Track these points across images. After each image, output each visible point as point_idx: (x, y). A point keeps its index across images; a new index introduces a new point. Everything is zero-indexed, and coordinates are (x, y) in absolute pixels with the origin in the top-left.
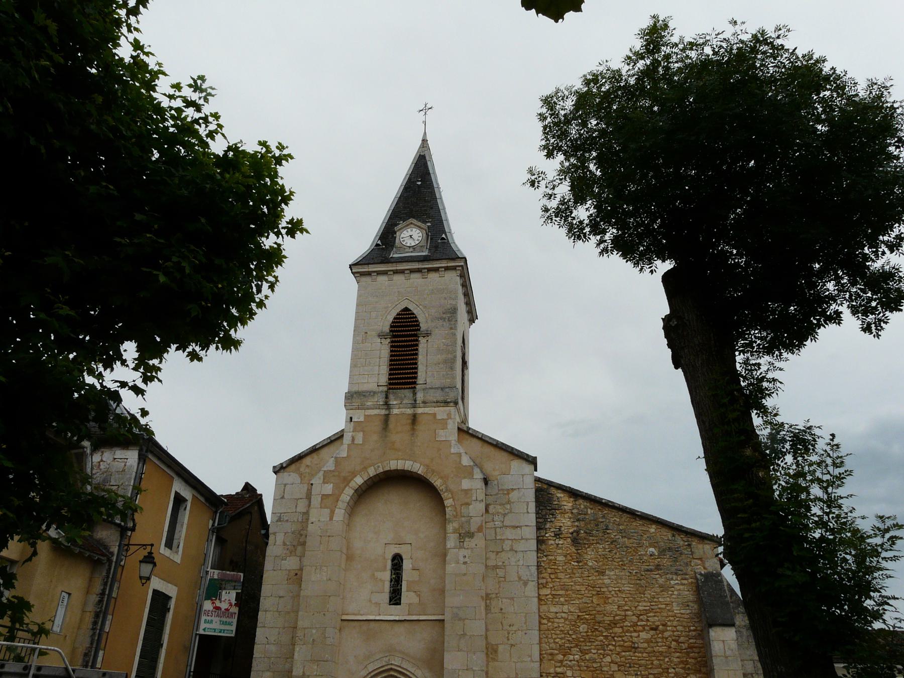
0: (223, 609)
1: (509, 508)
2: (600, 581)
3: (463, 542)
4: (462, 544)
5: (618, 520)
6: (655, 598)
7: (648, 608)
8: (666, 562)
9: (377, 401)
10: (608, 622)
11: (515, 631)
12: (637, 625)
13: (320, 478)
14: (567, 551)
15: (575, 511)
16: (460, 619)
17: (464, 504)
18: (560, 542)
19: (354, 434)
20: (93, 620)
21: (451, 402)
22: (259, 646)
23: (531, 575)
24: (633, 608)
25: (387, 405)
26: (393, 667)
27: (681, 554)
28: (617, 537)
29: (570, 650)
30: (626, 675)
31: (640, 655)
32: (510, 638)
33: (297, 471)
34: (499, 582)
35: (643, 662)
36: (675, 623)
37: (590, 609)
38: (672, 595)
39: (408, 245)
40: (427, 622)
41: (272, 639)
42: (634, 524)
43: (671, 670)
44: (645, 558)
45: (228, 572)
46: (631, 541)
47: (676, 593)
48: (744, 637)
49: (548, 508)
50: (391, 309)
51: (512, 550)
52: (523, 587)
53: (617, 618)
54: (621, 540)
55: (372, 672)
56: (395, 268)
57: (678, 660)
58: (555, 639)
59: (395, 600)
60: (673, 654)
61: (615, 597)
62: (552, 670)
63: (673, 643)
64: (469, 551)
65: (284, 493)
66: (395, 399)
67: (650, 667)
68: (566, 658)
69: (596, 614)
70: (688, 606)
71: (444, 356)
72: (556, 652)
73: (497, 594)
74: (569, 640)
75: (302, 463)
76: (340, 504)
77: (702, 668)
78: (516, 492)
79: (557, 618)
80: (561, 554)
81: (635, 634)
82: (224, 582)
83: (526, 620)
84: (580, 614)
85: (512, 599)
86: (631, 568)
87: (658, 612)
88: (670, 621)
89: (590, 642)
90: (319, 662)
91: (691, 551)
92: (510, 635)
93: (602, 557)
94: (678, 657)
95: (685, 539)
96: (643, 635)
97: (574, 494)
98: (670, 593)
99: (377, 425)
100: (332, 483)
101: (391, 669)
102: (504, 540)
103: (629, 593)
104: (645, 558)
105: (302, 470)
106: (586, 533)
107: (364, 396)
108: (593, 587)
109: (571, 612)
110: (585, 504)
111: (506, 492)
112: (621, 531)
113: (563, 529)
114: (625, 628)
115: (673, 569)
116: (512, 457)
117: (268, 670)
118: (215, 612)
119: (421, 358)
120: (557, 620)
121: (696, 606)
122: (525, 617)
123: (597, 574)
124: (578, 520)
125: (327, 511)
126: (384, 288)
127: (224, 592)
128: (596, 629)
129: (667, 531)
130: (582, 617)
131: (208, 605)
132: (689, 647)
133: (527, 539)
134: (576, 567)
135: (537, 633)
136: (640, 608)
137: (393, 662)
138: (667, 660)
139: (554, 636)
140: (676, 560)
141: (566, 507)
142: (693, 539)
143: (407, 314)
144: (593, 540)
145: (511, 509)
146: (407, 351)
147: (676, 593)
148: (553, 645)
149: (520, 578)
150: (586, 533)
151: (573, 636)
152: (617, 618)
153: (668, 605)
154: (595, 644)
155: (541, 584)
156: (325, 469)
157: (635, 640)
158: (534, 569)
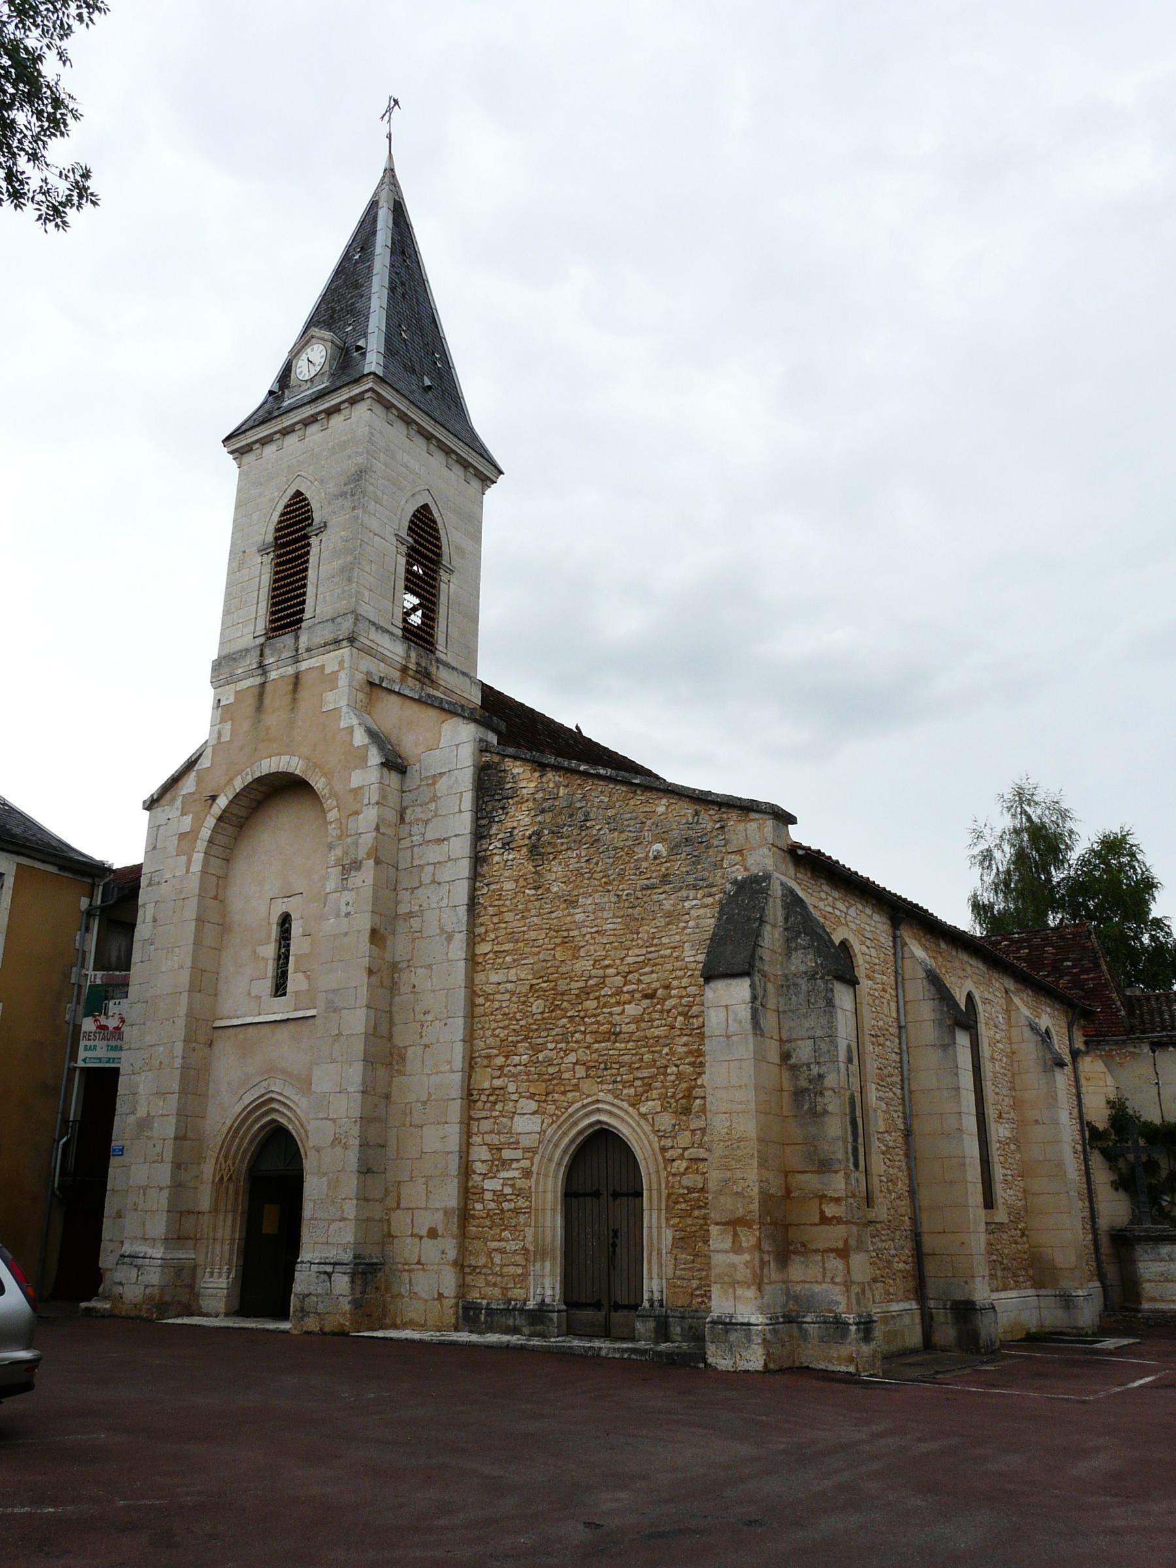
0: (111, 1029)
2: (568, 918)
5: (606, 800)
6: (653, 938)
7: (641, 958)
8: (679, 867)
9: (249, 665)
10: (576, 992)
11: (432, 1021)
12: (622, 992)
13: (177, 809)
14: (520, 870)
15: (539, 795)
16: (335, 1010)
17: (351, 815)
21: (343, 640)
26: (600, 1106)
27: (708, 848)
31: (623, 1045)
34: (413, 940)
35: (626, 1058)
38: (685, 928)
45: (118, 973)
46: (624, 836)
47: (691, 924)
48: (802, 996)
49: (497, 797)
51: (433, 881)
52: (446, 943)
53: (591, 982)
57: (685, 1049)
58: (494, 1029)
60: (677, 1038)
61: (591, 944)
62: (486, 1085)
64: (353, 893)
66: (272, 655)
67: (636, 1066)
68: (509, 1062)
69: (558, 978)
73: (409, 961)
74: (514, 1030)
78: (445, 778)
79: (498, 993)
81: (618, 1009)
82: (110, 989)
84: (535, 982)
94: (685, 1045)
95: (716, 818)
96: (631, 1009)
98: (682, 925)
103: (614, 935)
104: (645, 864)
106: (553, 833)
108: (557, 932)
109: (521, 980)
110: (557, 778)
111: (430, 782)
115: (690, 879)
116: (443, 716)
118: (100, 1033)
119: (311, 574)
120: (498, 997)
123: (563, 906)
124: (543, 811)
125: (184, 858)
126: (270, 466)
127: (111, 1003)
130: (537, 987)
131: (88, 1025)
134: (532, 898)
136: (630, 960)
138: (666, 1050)
139: (494, 1025)
140: (696, 860)
144: (562, 844)
149: (442, 929)
150: (553, 833)
151: (522, 1023)
152: (591, 982)
154: (554, 1033)
155: (479, 935)
156: (184, 792)
158: (462, 911)
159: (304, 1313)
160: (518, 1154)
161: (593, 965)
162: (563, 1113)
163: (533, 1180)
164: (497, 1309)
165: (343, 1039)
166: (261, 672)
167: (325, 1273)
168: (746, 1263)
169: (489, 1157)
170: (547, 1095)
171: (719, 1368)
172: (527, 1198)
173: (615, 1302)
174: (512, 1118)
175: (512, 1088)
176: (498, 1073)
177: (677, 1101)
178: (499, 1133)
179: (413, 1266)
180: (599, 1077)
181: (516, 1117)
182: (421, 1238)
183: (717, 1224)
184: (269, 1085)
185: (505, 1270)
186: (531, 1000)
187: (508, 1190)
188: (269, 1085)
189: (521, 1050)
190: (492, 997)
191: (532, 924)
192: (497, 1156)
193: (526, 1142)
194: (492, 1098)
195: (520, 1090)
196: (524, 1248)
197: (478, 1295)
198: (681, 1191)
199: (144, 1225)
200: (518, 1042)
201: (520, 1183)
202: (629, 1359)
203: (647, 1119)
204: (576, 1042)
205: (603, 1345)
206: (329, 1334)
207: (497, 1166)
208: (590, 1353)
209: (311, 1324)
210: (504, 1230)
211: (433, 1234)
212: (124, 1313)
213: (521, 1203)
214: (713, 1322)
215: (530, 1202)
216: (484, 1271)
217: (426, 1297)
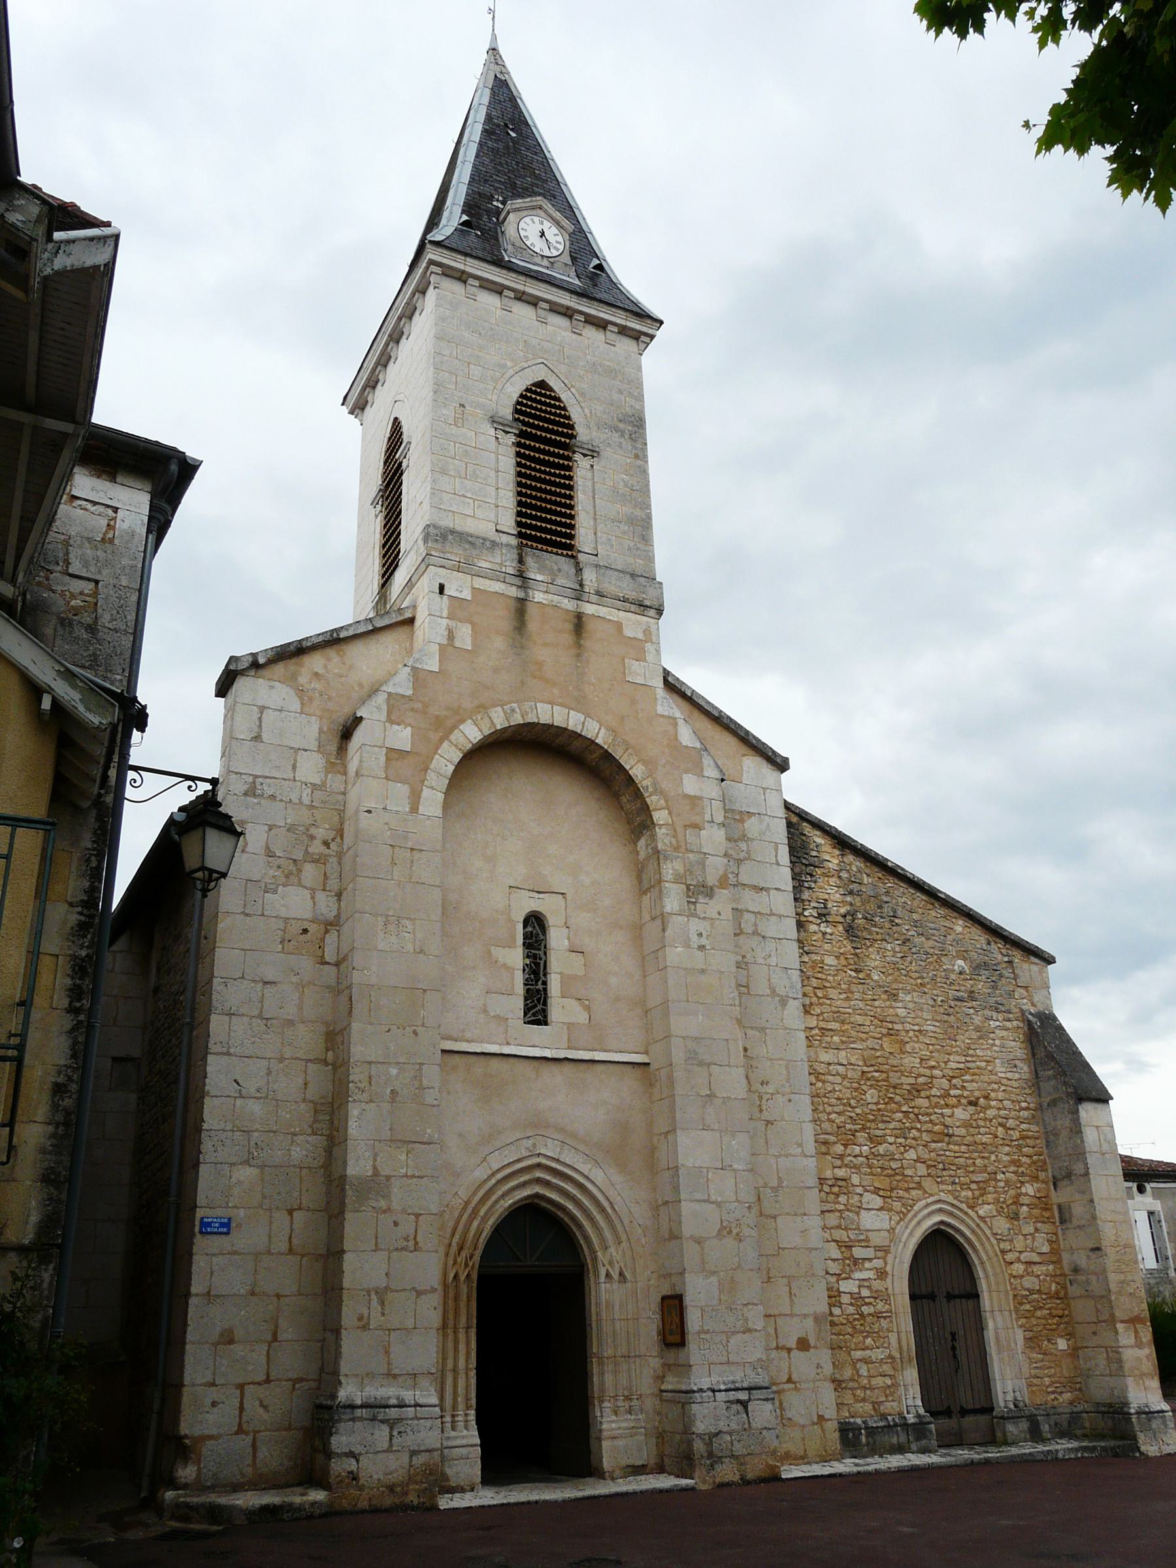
1: (745, 849)
3: (694, 903)
4: (693, 907)
6: (969, 1048)
7: (962, 1066)
8: (981, 987)
10: (908, 1088)
11: (772, 1094)
12: (949, 1094)
14: (840, 948)
16: (701, 1064)
18: (829, 930)
19: (453, 624)
20: (69, 981)
21: (651, 607)
22: (216, 1101)
23: (792, 987)
24: (943, 1065)
28: (910, 933)
29: (854, 1136)
30: (938, 1183)
31: (957, 1148)
32: (764, 1108)
33: (291, 681)
36: (1000, 1095)
37: (880, 1060)
40: (611, 1066)
41: (251, 1087)
42: (933, 913)
43: (1000, 1176)
44: (953, 976)
46: (931, 943)
47: (997, 1042)
50: (511, 372)
53: (921, 1080)
54: (917, 940)
55: (498, 1171)
56: (520, 287)
58: (829, 1114)
59: (534, 1015)
62: (828, 1174)
63: (1000, 1129)
64: (707, 924)
65: (260, 726)
66: (541, 570)
67: (971, 1169)
68: (848, 1151)
70: (1015, 1066)
71: (627, 510)
74: (851, 1117)
75: (302, 666)
76: (431, 777)
77: (1040, 1173)
80: (830, 953)
81: (947, 1111)
84: (866, 1069)
85: (762, 1030)
86: (934, 992)
87: (976, 1074)
88: (993, 1090)
89: (883, 1122)
90: (411, 1146)
91: (1013, 972)
92: (764, 1101)
93: (893, 966)
95: (1004, 951)
97: (842, 842)
98: (991, 1042)
99: (501, 618)
100: (410, 725)
101: (539, 1166)
105: (303, 680)
106: (866, 919)
108: (881, 1021)
109: (851, 1064)
110: (858, 863)
111: (738, 817)
112: (915, 924)
113: (829, 905)
114: (934, 1100)
116: (744, 749)
117: (247, 1162)
119: (581, 498)
120: (830, 1078)
121: (1026, 1068)
123: (884, 997)
124: (851, 893)
128: (891, 1098)
129: (979, 933)
130: (870, 1075)
132: (1023, 1138)
133: (780, 916)
135: (808, 1100)
136: (953, 1065)
137: (543, 1151)
138: (993, 1158)
139: (829, 1109)
141: (830, 865)
142: (1014, 953)
143: (540, 394)
144: (877, 933)
145: (748, 852)
146: (549, 474)
147: (997, 1042)
148: (826, 1125)
151: (858, 1111)
153: (988, 1062)
154: (891, 1126)
157: (948, 1121)
159: (714, 1459)
160: (869, 1252)
161: (920, 1063)
162: (909, 1211)
163: (889, 1280)
164: (877, 1427)
165: (718, 1102)
166: (520, 583)
167: (739, 1401)
168: (1148, 1357)
170: (892, 1190)
171: (1150, 1454)
172: (887, 1301)
173: (961, 1407)
174: (858, 1214)
175: (855, 1180)
176: (838, 1163)
177: (1008, 1206)
178: (846, 1229)
179: (781, 1387)
180: (938, 1177)
181: (863, 1213)
182: (789, 1350)
183: (1122, 1322)
184: (534, 1145)
185: (874, 1382)
186: (864, 1087)
187: (865, 1293)
188: (534, 1145)
189: (861, 1140)
190: (823, 1077)
191: (857, 1007)
192: (847, 1254)
193: (877, 1239)
194: (836, 1189)
195: (865, 1183)
196: (890, 1356)
197: (847, 1414)
198: (1025, 1293)
199: (387, 1353)
200: (856, 1131)
201: (877, 1285)
202: (1083, 1457)
203: (985, 1222)
204: (913, 1139)
205: (1059, 1447)
207: (849, 1265)
208: (1049, 1458)
209: (727, 1472)
210: (867, 1337)
212: (364, 1504)
213: (880, 1306)
214: (1138, 1413)
215: (890, 1304)
216: (851, 1385)
217: (802, 1421)
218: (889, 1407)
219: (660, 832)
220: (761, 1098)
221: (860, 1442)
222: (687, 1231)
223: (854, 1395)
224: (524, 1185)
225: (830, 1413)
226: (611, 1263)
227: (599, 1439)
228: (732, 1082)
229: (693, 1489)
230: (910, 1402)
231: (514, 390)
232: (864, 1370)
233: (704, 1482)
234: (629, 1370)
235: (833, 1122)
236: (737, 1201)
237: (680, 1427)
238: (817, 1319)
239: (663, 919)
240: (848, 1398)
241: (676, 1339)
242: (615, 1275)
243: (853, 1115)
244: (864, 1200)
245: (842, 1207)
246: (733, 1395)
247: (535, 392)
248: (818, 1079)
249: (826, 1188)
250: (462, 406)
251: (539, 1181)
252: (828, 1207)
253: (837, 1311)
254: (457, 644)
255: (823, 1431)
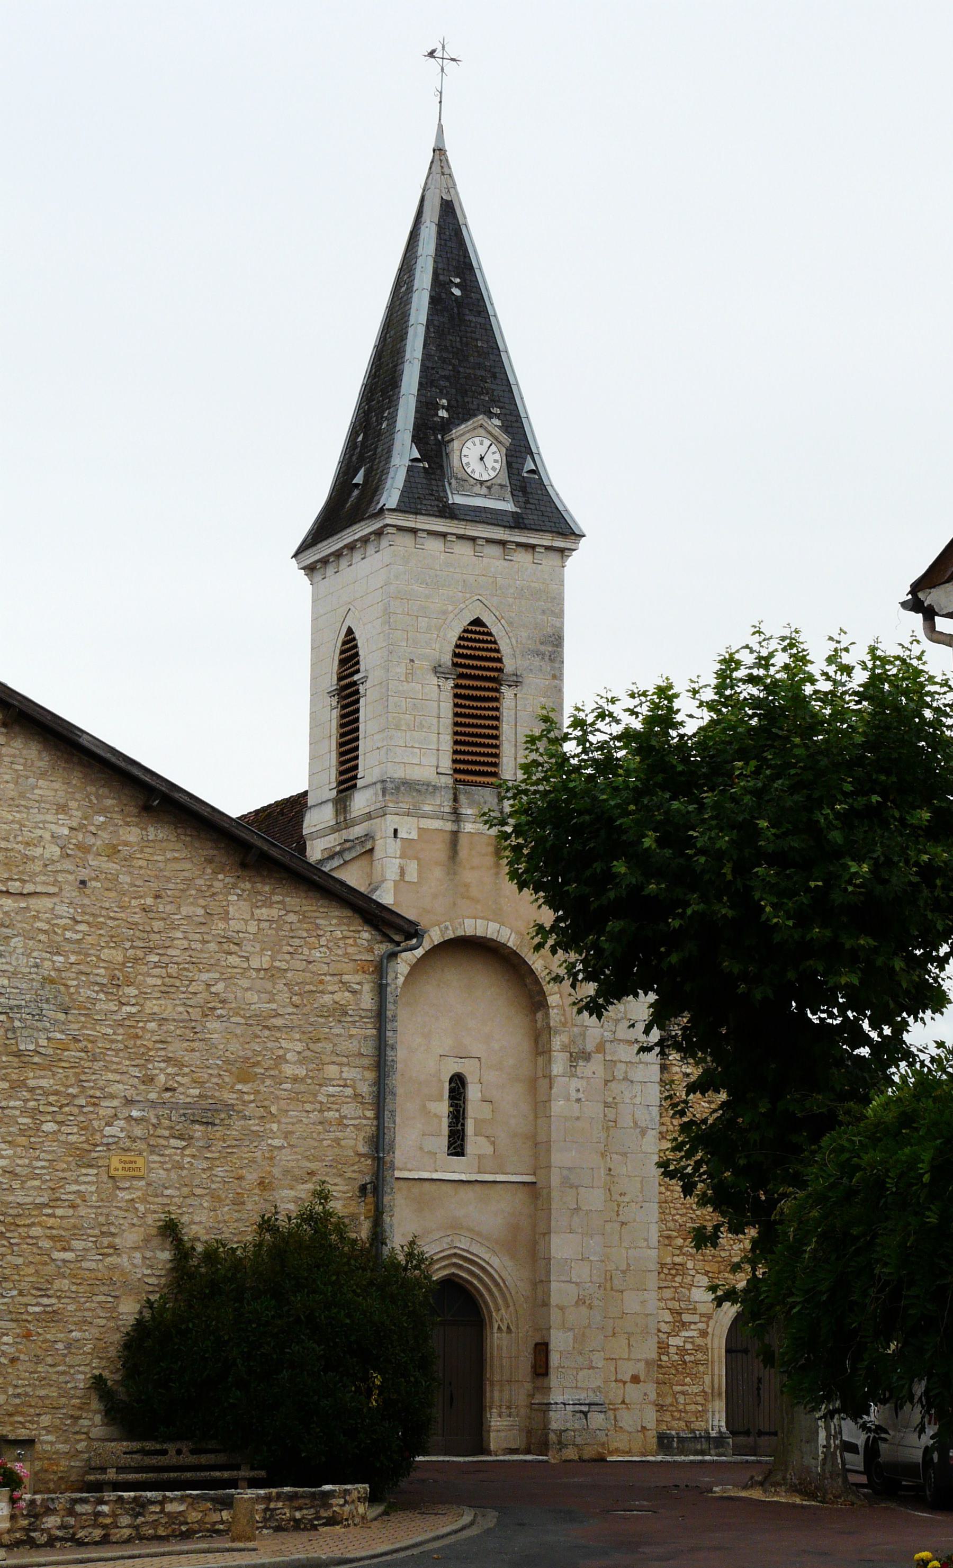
1: (622, 1010)
4: (574, 1069)
9: (440, 805)
16: (571, 1187)
19: (402, 861)
23: (652, 1120)
25: (456, 815)
39: (477, 476)
51: (626, 1079)
58: (674, 1215)
59: (454, 1148)
62: (669, 1260)
64: (584, 1083)
66: (470, 806)
72: (675, 1234)
83: (642, 1186)
85: (624, 1154)
92: (621, 1208)
99: (439, 850)
101: (455, 1255)
102: (615, 1062)
107: (419, 791)
122: (642, 1182)
135: (656, 1206)
139: (673, 1212)
145: (625, 1012)
149: (635, 1123)
159: (562, 1445)
160: (696, 1318)
166: (454, 819)
167: (581, 1412)
169: (671, 1319)
170: (719, 1273)
174: (689, 1290)
175: (690, 1265)
176: (678, 1252)
178: (679, 1300)
181: (694, 1290)
184: (452, 1241)
185: (688, 1408)
187: (688, 1346)
194: (673, 1272)
195: (697, 1267)
201: (699, 1341)
206: (588, 1461)
209: (570, 1453)
211: (635, 1379)
213: (700, 1356)
216: (670, 1408)
218: (699, 1425)
219: (553, 1013)
220: (619, 1206)
221: (672, 1445)
222: (553, 1301)
223: (672, 1416)
224: (444, 1267)
225: (651, 1424)
226: (502, 1320)
227: (489, 1431)
228: (594, 1199)
229: (547, 1461)
230: (716, 1423)
231: (453, 635)
232: (681, 1399)
233: (554, 1458)
234: (511, 1390)
235: (677, 1221)
236: (591, 1282)
237: (542, 1427)
238: (648, 1363)
239: (550, 1078)
240: (667, 1417)
241: (542, 1371)
242: (504, 1328)
243: (694, 1216)
244: (696, 1279)
245: (677, 1285)
246: (578, 1408)
247: (471, 632)
248: (667, 1189)
249: (666, 1271)
250: (412, 661)
251: (455, 1265)
252: (666, 1284)
253: (664, 1358)
254: (407, 879)
255: (645, 1437)
